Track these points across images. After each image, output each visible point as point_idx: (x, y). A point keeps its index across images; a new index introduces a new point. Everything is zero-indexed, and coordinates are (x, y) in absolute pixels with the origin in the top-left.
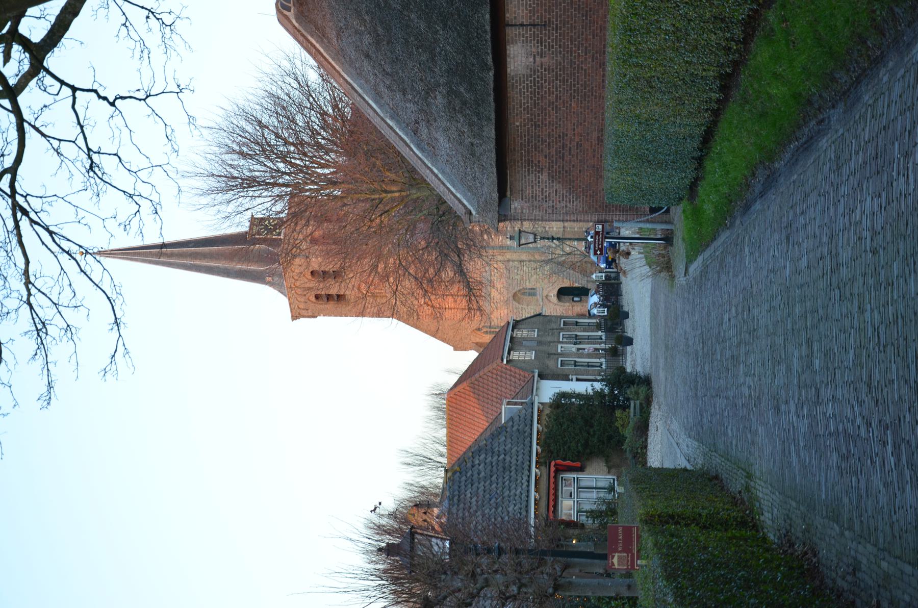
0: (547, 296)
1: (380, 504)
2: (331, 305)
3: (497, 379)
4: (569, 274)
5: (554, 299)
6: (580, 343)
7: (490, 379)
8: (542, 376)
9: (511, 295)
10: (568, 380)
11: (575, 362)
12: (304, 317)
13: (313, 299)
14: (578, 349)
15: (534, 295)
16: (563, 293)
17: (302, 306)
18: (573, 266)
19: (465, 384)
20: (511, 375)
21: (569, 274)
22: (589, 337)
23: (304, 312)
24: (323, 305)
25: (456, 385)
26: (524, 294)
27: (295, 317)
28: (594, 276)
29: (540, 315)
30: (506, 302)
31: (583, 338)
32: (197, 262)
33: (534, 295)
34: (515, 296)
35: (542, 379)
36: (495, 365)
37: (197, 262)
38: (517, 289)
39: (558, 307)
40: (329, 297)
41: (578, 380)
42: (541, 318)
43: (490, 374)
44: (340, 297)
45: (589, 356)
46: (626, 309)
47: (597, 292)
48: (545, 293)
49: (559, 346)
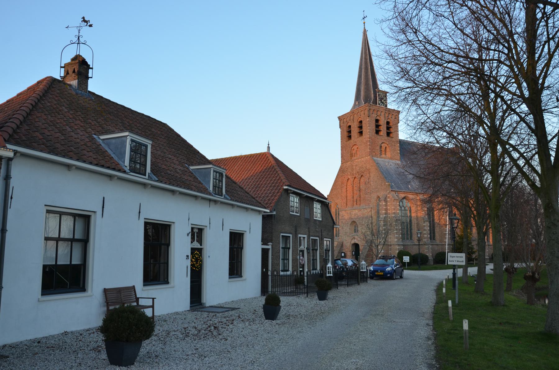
0: (354, 238)
1: (91, 26)
2: (346, 134)
3: (273, 183)
4: (366, 248)
5: (353, 242)
6: (308, 253)
7: (274, 179)
8: (266, 219)
9: (354, 220)
10: (265, 241)
11: (329, 250)
12: (340, 122)
13: (348, 125)
14: (302, 251)
15: (355, 232)
16: (356, 246)
17: (345, 120)
18: (370, 250)
19: (273, 162)
20: (274, 193)
21: (366, 248)
22: (314, 260)
23: (342, 122)
24: (346, 129)
25: (272, 156)
26: (355, 227)
27: (339, 118)
28: (363, 262)
29: (334, 223)
30: (351, 218)
31: (314, 255)
32: (363, 70)
33: (355, 232)
34: (354, 222)
35: (264, 217)
36: (284, 181)
37: (363, 70)
38: (358, 223)
39: (349, 244)
40: (350, 132)
41: (265, 253)
42: (332, 224)
43: (278, 178)
44: (350, 137)
45: (295, 260)
46: (331, 294)
47: (354, 264)
48: (356, 237)
49: (306, 236)
